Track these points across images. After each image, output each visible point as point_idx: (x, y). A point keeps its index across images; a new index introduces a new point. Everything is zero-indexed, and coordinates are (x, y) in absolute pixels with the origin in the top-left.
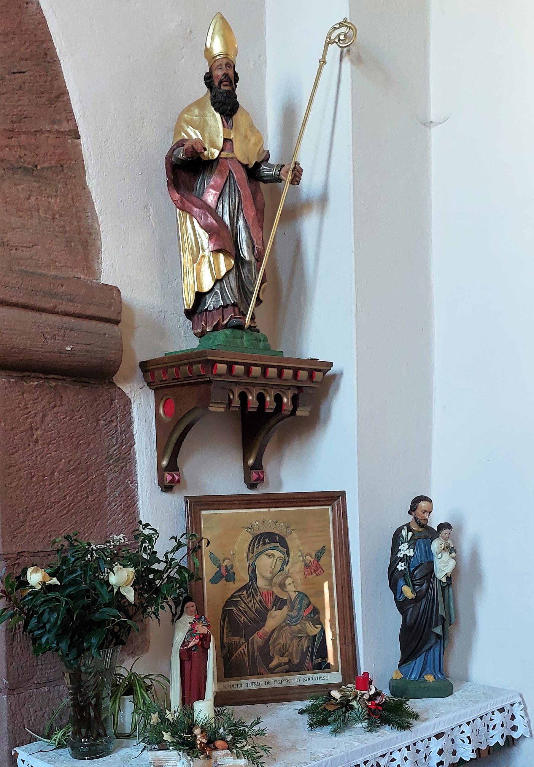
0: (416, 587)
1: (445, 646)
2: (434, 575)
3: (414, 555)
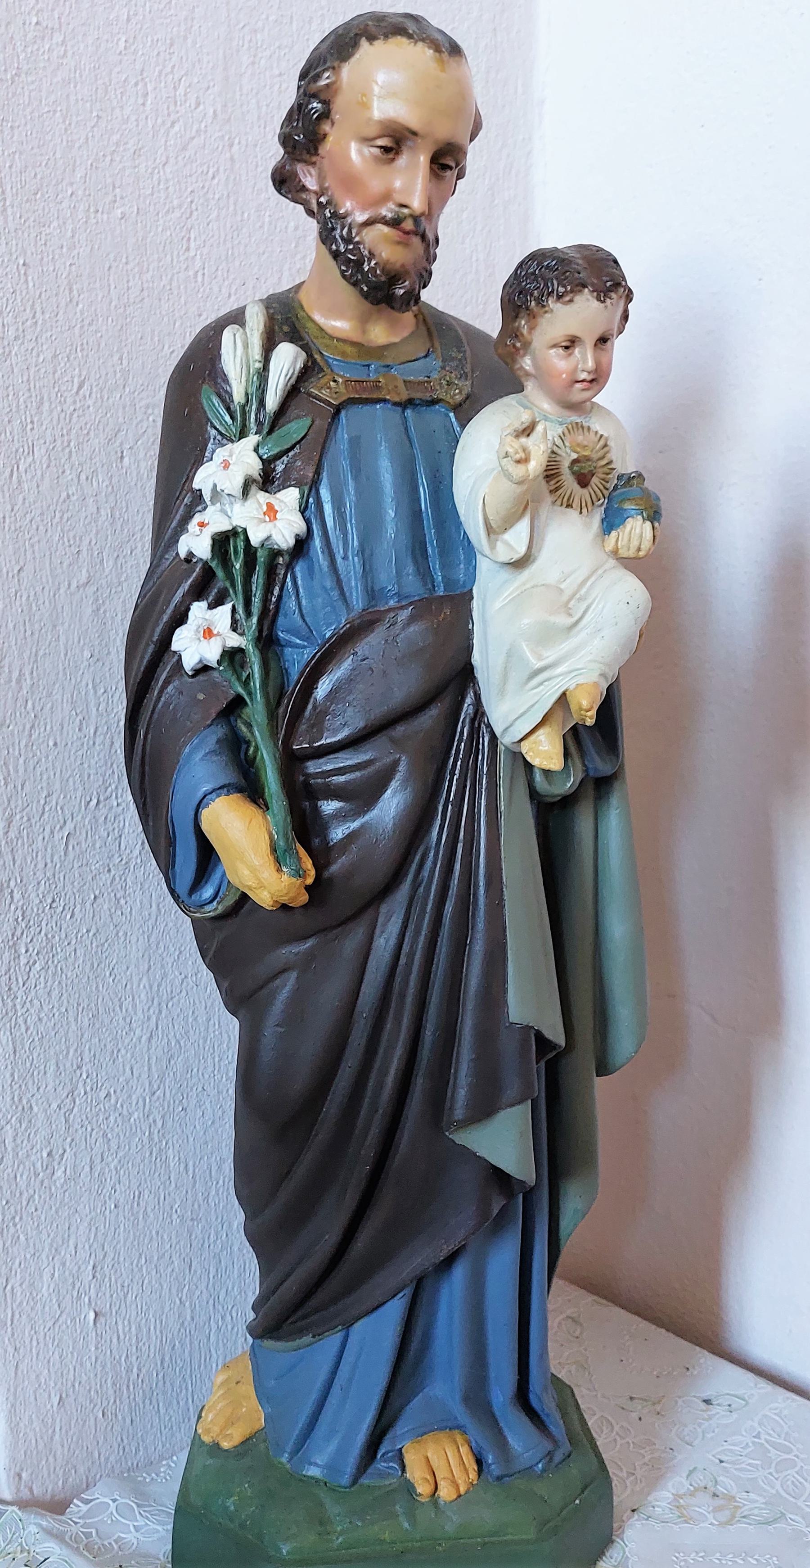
0: (329, 807)
1: (565, 1223)
2: (479, 712)
3: (301, 545)
